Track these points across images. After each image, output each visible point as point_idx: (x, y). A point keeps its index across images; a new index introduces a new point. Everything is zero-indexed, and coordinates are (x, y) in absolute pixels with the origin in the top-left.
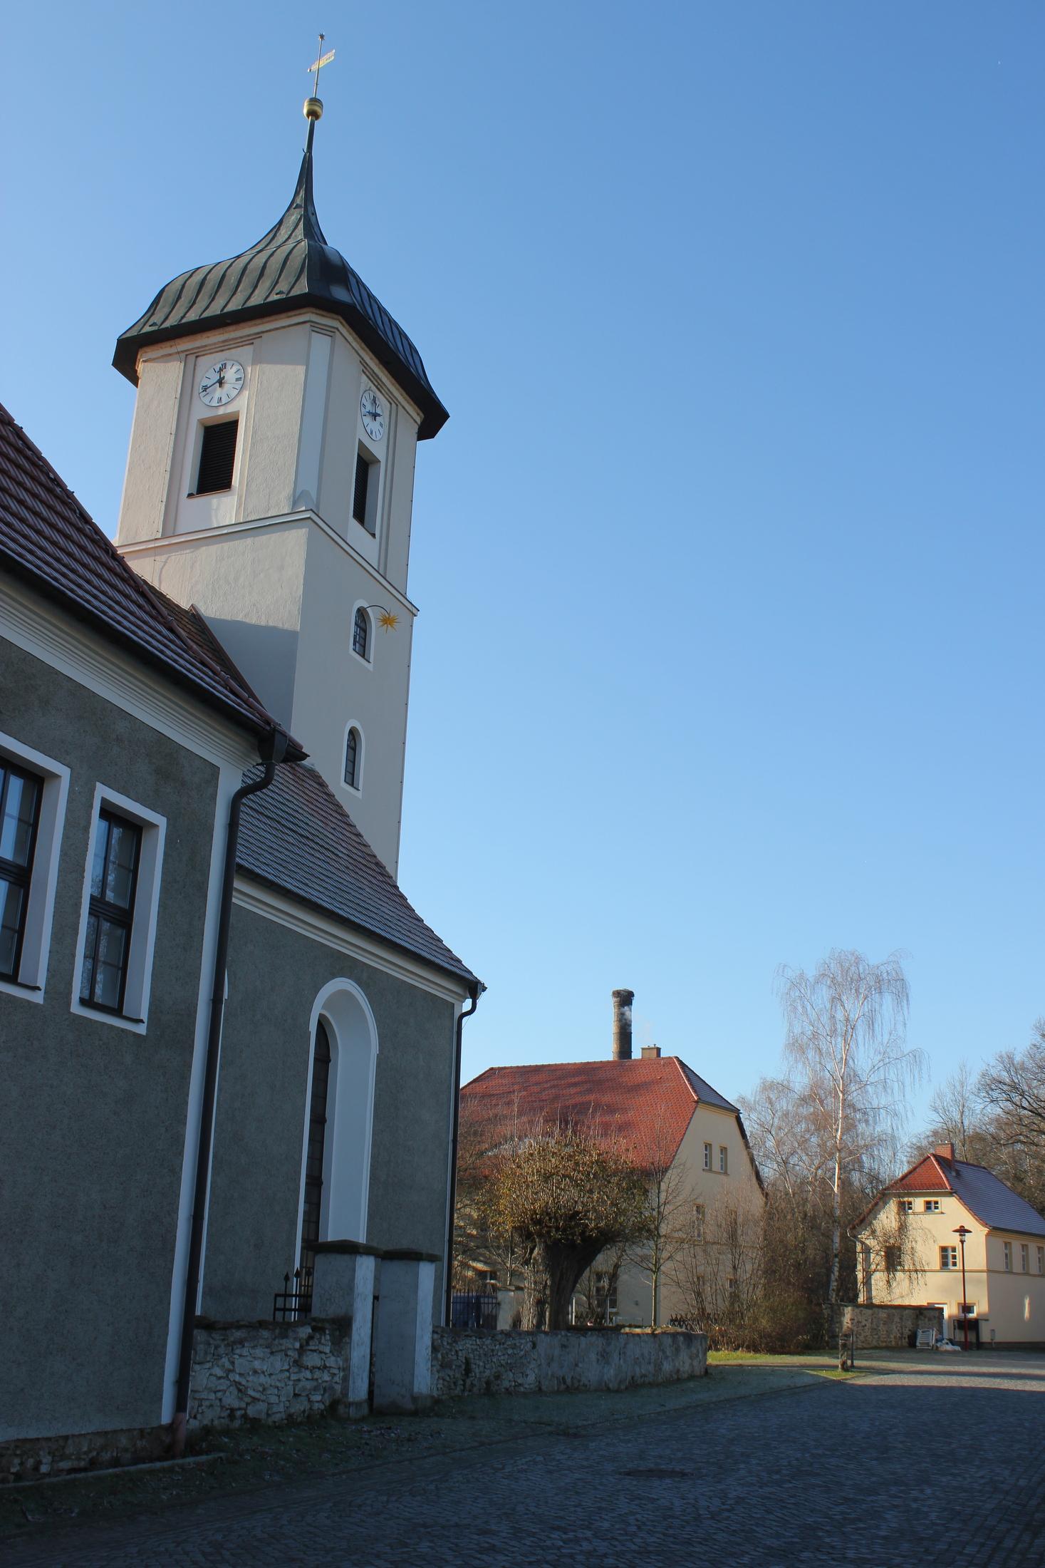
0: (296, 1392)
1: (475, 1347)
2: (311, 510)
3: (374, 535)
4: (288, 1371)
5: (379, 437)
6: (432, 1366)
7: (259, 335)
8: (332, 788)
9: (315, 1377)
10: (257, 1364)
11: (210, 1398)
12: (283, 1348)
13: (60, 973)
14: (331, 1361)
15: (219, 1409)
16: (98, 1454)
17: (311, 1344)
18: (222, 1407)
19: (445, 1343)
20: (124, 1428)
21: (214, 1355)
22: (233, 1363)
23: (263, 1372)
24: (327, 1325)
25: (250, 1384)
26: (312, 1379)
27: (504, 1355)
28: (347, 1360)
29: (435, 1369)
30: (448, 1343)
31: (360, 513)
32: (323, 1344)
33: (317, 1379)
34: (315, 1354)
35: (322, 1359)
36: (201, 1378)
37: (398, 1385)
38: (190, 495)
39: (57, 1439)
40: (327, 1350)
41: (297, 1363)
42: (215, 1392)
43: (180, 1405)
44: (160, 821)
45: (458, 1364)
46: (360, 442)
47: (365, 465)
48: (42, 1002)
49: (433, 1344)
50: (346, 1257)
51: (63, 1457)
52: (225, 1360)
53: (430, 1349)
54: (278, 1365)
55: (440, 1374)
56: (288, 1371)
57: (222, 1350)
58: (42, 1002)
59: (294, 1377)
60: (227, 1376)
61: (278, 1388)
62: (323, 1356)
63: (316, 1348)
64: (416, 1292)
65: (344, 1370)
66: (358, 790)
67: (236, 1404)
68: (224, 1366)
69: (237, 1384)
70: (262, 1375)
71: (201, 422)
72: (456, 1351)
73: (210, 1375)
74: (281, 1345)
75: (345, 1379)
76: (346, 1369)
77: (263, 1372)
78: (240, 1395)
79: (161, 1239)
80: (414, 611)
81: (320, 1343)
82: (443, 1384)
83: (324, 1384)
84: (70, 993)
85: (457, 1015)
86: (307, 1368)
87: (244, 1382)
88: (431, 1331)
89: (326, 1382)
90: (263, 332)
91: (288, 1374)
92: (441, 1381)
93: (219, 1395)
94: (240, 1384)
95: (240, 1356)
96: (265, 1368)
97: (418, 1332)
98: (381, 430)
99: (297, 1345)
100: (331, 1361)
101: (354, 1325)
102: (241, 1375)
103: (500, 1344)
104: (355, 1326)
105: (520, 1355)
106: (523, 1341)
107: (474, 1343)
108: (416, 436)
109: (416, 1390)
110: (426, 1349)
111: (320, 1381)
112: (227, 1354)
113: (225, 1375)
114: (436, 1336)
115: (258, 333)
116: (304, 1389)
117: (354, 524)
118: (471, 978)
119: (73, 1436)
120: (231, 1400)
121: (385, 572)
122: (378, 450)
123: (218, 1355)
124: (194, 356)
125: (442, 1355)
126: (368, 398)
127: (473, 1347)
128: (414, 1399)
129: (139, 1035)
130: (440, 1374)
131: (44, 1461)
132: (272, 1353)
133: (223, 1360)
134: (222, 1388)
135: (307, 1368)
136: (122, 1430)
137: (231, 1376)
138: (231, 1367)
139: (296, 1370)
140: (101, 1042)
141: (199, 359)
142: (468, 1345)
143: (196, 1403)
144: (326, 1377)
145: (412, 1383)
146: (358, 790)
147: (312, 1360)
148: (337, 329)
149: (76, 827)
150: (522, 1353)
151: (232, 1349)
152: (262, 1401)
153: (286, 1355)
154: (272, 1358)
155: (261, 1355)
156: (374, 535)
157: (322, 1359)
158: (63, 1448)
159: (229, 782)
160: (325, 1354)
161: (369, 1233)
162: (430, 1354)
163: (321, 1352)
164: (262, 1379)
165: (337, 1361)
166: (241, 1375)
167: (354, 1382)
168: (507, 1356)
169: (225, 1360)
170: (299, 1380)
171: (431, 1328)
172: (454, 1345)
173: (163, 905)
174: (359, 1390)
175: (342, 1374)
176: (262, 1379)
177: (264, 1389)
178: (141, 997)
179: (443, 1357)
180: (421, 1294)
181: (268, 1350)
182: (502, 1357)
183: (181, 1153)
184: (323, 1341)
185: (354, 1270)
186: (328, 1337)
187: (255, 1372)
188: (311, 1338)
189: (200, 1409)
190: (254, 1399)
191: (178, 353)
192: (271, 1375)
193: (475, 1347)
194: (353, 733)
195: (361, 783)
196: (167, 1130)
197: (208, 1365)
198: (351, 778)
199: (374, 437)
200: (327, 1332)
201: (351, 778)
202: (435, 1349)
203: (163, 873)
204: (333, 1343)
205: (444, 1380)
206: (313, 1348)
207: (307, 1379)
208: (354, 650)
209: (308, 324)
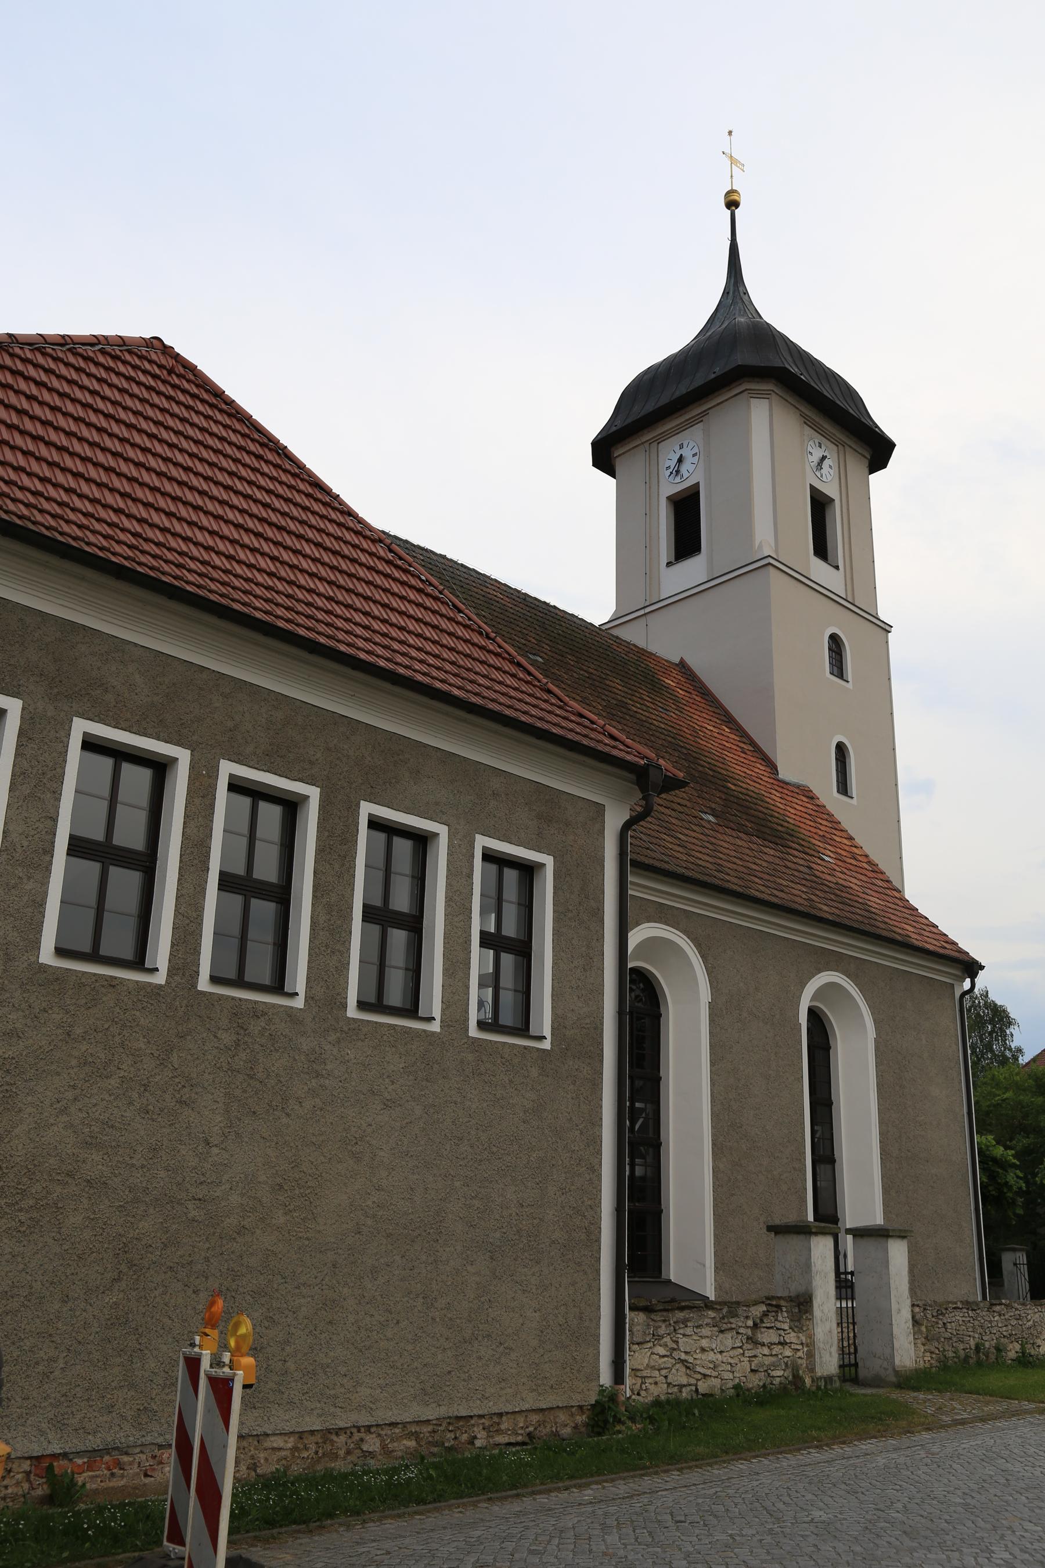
0: (753, 1368)
1: (968, 1319)
2: (769, 556)
3: (837, 568)
4: (741, 1347)
5: (830, 478)
6: (915, 1339)
7: (705, 413)
8: (823, 800)
9: (774, 1353)
10: (704, 1343)
11: (653, 1375)
12: (733, 1326)
13: (455, 1000)
14: (791, 1337)
15: (666, 1385)
16: (535, 1429)
17: (765, 1321)
18: (669, 1384)
19: (929, 1316)
20: (561, 1405)
21: (653, 1335)
22: (677, 1342)
23: (713, 1350)
24: (783, 1303)
25: (698, 1362)
26: (771, 1355)
27: (1006, 1326)
28: (811, 1336)
29: (919, 1341)
30: (933, 1316)
31: (821, 549)
32: (780, 1322)
33: (776, 1355)
34: (771, 1331)
35: (780, 1335)
36: (635, 1359)
37: (879, 1358)
38: (669, 564)
39: (492, 1415)
40: (786, 1326)
41: (751, 1340)
42: (659, 1370)
43: (618, 1377)
44: (548, 860)
45: (946, 1336)
46: (811, 486)
47: (820, 505)
48: (439, 1030)
49: (913, 1317)
50: (802, 1237)
51: (499, 1431)
52: (667, 1339)
53: (910, 1324)
54: (729, 1343)
55: (926, 1347)
56: (741, 1347)
57: (662, 1331)
58: (439, 1030)
59: (748, 1354)
60: (671, 1355)
61: (731, 1364)
62: (782, 1332)
63: (773, 1325)
64: (887, 1267)
65: (807, 1346)
66: (852, 798)
67: (684, 1380)
68: (667, 1345)
69: (683, 1362)
70: (712, 1353)
71: (668, 498)
72: (944, 1324)
73: (652, 1353)
74: (731, 1323)
75: (810, 1355)
76: (810, 1346)
77: (713, 1350)
78: (688, 1371)
79: (584, 1230)
80: (887, 628)
81: (776, 1320)
82: (932, 1358)
83: (786, 1360)
84: (467, 1020)
85: (958, 994)
86: (763, 1345)
87: (691, 1360)
88: (910, 1305)
89: (788, 1357)
90: (709, 409)
91: (741, 1351)
92: (928, 1354)
93: (664, 1372)
94: (686, 1361)
95: (684, 1335)
96: (714, 1346)
97: (894, 1306)
98: (832, 472)
99: (750, 1323)
100: (791, 1337)
101: (814, 1302)
102: (686, 1353)
103: (1000, 1315)
104: (816, 1303)
105: (1027, 1326)
106: (1030, 1312)
107: (966, 1315)
108: (867, 471)
109: (897, 1362)
110: (906, 1322)
111: (780, 1356)
112: (669, 1334)
113: (668, 1353)
114: (917, 1309)
115: (705, 411)
116: (762, 1365)
117: (817, 563)
118: (966, 958)
119: (507, 1413)
120: (680, 1377)
121: (854, 598)
122: (830, 490)
123: (659, 1336)
124: (656, 443)
125: (926, 1327)
126: (813, 446)
127: (964, 1319)
128: (897, 1373)
129: (544, 1050)
130: (926, 1347)
131: (479, 1436)
132: (722, 1332)
133: (665, 1340)
134: (667, 1366)
135: (763, 1345)
136: (558, 1407)
137: (675, 1354)
138: (676, 1347)
139: (749, 1346)
140: (503, 1060)
141: (660, 445)
142: (958, 1318)
143: (639, 1381)
144: (788, 1352)
145: (893, 1356)
146: (852, 798)
147: (767, 1336)
148: (773, 391)
149: (459, 874)
150: (1031, 1323)
151: (675, 1330)
152: (715, 1377)
153: (738, 1333)
154: (721, 1335)
155: (709, 1334)
156: (837, 568)
157: (780, 1335)
158: (498, 1424)
159: (614, 820)
160: (784, 1330)
161: (720, 1266)
162: (911, 1327)
163: (778, 1329)
164: (711, 1356)
165: (799, 1337)
166: (686, 1353)
167: (821, 1357)
168: (1010, 1327)
169: (667, 1339)
170: (755, 1356)
171: (908, 1302)
172: (941, 1317)
173: (556, 932)
174: (829, 1363)
175: (805, 1349)
176: (711, 1356)
177: (715, 1367)
178: (544, 1020)
179: (927, 1330)
180: (892, 1269)
181: (716, 1329)
182: (1004, 1329)
183: (599, 1152)
184: (780, 1318)
185: (810, 1250)
186: (785, 1315)
187: (703, 1350)
188: (765, 1314)
189: (644, 1387)
190: (705, 1376)
191: (643, 443)
192: (721, 1352)
193: (968, 1319)
194: (841, 750)
195: (854, 789)
196: (581, 1133)
197: (650, 1345)
198: (843, 787)
199: (824, 479)
200: (784, 1309)
201: (843, 787)
202: (916, 1322)
203: (555, 904)
204: (791, 1320)
205: (932, 1353)
206: (768, 1325)
207: (765, 1355)
208: (832, 673)
209: (746, 392)
